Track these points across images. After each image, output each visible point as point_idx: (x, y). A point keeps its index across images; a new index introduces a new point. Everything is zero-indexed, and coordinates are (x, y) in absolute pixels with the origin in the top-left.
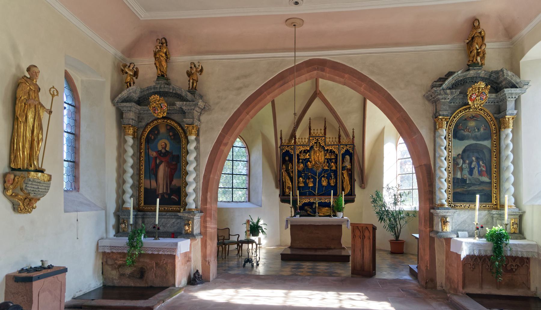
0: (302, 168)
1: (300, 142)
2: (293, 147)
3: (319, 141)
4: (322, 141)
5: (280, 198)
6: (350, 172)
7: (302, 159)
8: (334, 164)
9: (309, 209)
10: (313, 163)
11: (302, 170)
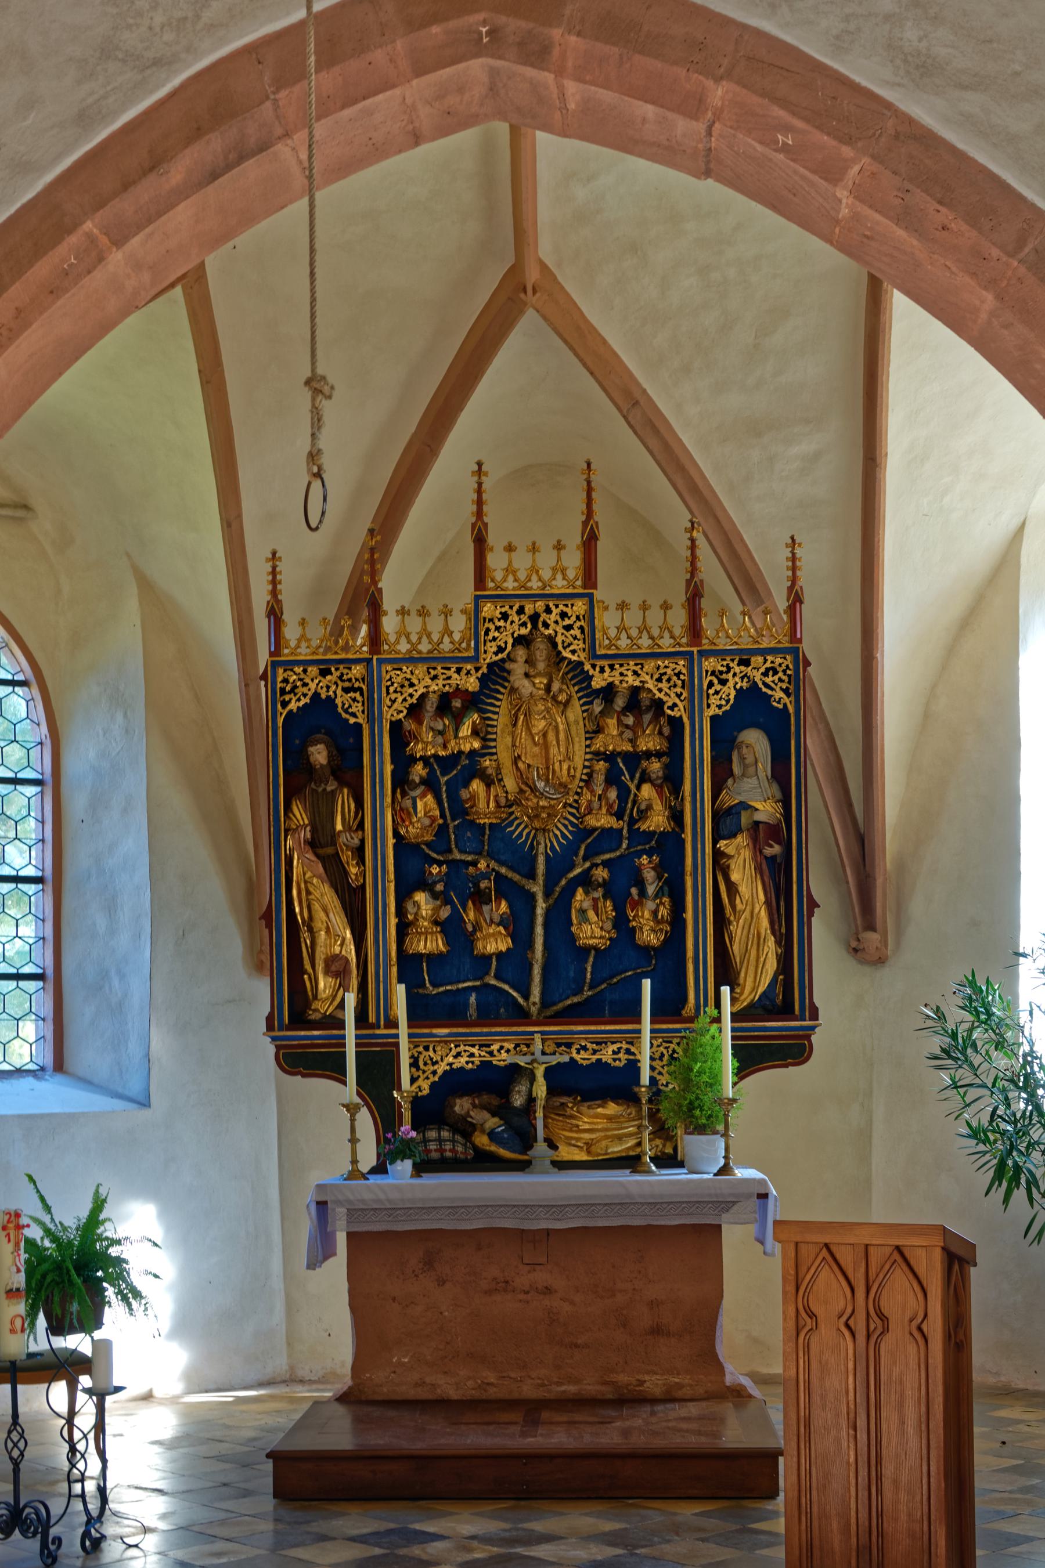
0: (427, 822)
1: (409, 641)
2: (357, 671)
3: (546, 625)
4: (568, 628)
5: (274, 1039)
6: (776, 849)
7: (425, 760)
8: (659, 789)
9: (486, 1115)
10: (510, 783)
11: (429, 838)
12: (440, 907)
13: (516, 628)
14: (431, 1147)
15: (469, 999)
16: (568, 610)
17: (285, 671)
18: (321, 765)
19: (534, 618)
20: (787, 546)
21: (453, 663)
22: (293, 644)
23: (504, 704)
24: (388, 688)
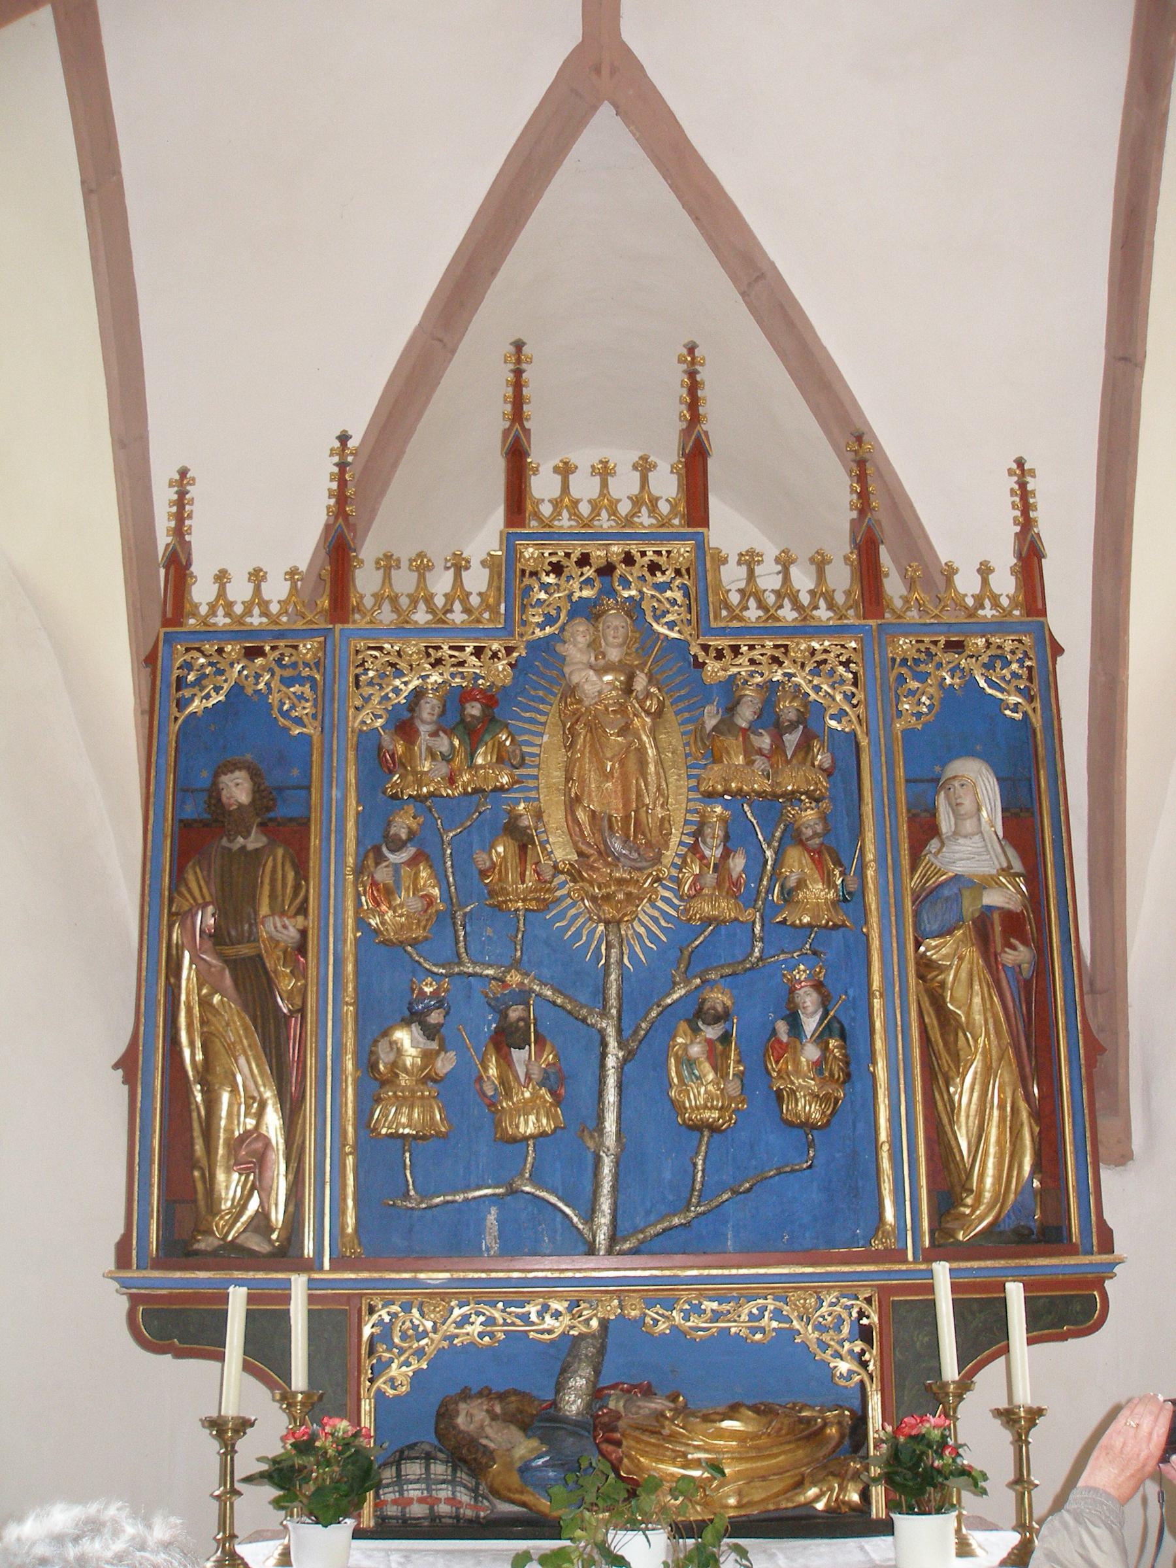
2: (307, 648)
5: (124, 1284)
9: (514, 1433)
12: (438, 1053)
13: (576, 586)
14: (412, 1494)
15: (485, 1219)
16: (662, 561)
17: (188, 650)
18: (240, 806)
19: (607, 570)
20: (1011, 472)
21: (468, 639)
22: (204, 610)
23: (553, 719)
24: (357, 677)
